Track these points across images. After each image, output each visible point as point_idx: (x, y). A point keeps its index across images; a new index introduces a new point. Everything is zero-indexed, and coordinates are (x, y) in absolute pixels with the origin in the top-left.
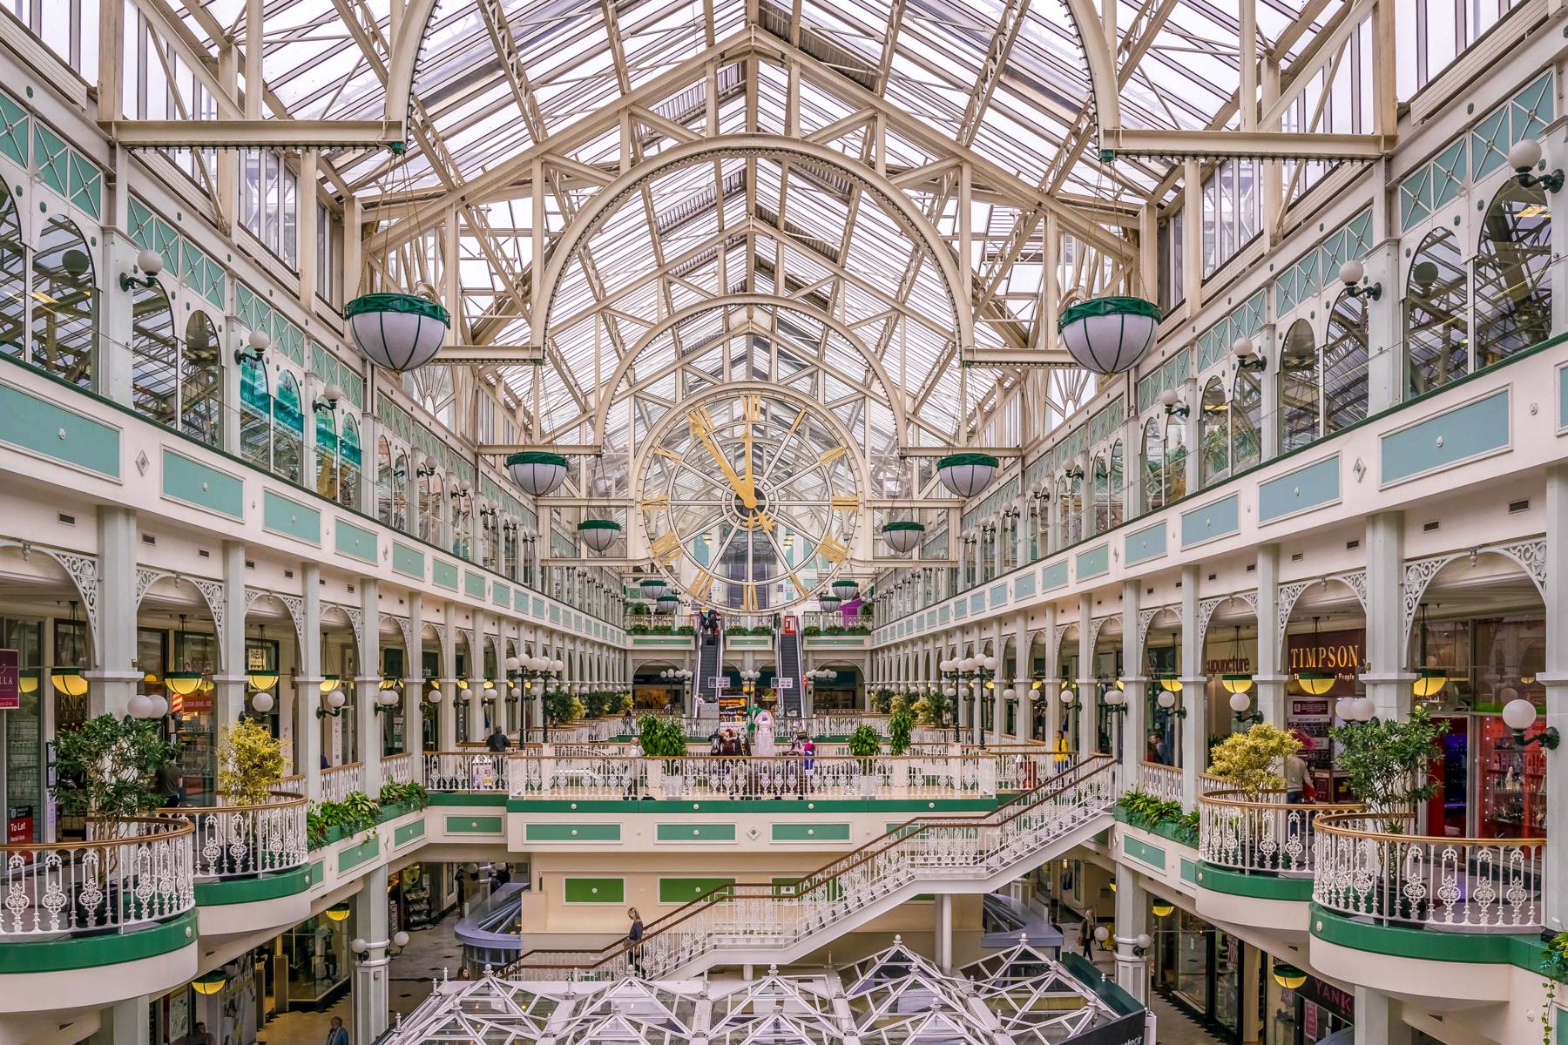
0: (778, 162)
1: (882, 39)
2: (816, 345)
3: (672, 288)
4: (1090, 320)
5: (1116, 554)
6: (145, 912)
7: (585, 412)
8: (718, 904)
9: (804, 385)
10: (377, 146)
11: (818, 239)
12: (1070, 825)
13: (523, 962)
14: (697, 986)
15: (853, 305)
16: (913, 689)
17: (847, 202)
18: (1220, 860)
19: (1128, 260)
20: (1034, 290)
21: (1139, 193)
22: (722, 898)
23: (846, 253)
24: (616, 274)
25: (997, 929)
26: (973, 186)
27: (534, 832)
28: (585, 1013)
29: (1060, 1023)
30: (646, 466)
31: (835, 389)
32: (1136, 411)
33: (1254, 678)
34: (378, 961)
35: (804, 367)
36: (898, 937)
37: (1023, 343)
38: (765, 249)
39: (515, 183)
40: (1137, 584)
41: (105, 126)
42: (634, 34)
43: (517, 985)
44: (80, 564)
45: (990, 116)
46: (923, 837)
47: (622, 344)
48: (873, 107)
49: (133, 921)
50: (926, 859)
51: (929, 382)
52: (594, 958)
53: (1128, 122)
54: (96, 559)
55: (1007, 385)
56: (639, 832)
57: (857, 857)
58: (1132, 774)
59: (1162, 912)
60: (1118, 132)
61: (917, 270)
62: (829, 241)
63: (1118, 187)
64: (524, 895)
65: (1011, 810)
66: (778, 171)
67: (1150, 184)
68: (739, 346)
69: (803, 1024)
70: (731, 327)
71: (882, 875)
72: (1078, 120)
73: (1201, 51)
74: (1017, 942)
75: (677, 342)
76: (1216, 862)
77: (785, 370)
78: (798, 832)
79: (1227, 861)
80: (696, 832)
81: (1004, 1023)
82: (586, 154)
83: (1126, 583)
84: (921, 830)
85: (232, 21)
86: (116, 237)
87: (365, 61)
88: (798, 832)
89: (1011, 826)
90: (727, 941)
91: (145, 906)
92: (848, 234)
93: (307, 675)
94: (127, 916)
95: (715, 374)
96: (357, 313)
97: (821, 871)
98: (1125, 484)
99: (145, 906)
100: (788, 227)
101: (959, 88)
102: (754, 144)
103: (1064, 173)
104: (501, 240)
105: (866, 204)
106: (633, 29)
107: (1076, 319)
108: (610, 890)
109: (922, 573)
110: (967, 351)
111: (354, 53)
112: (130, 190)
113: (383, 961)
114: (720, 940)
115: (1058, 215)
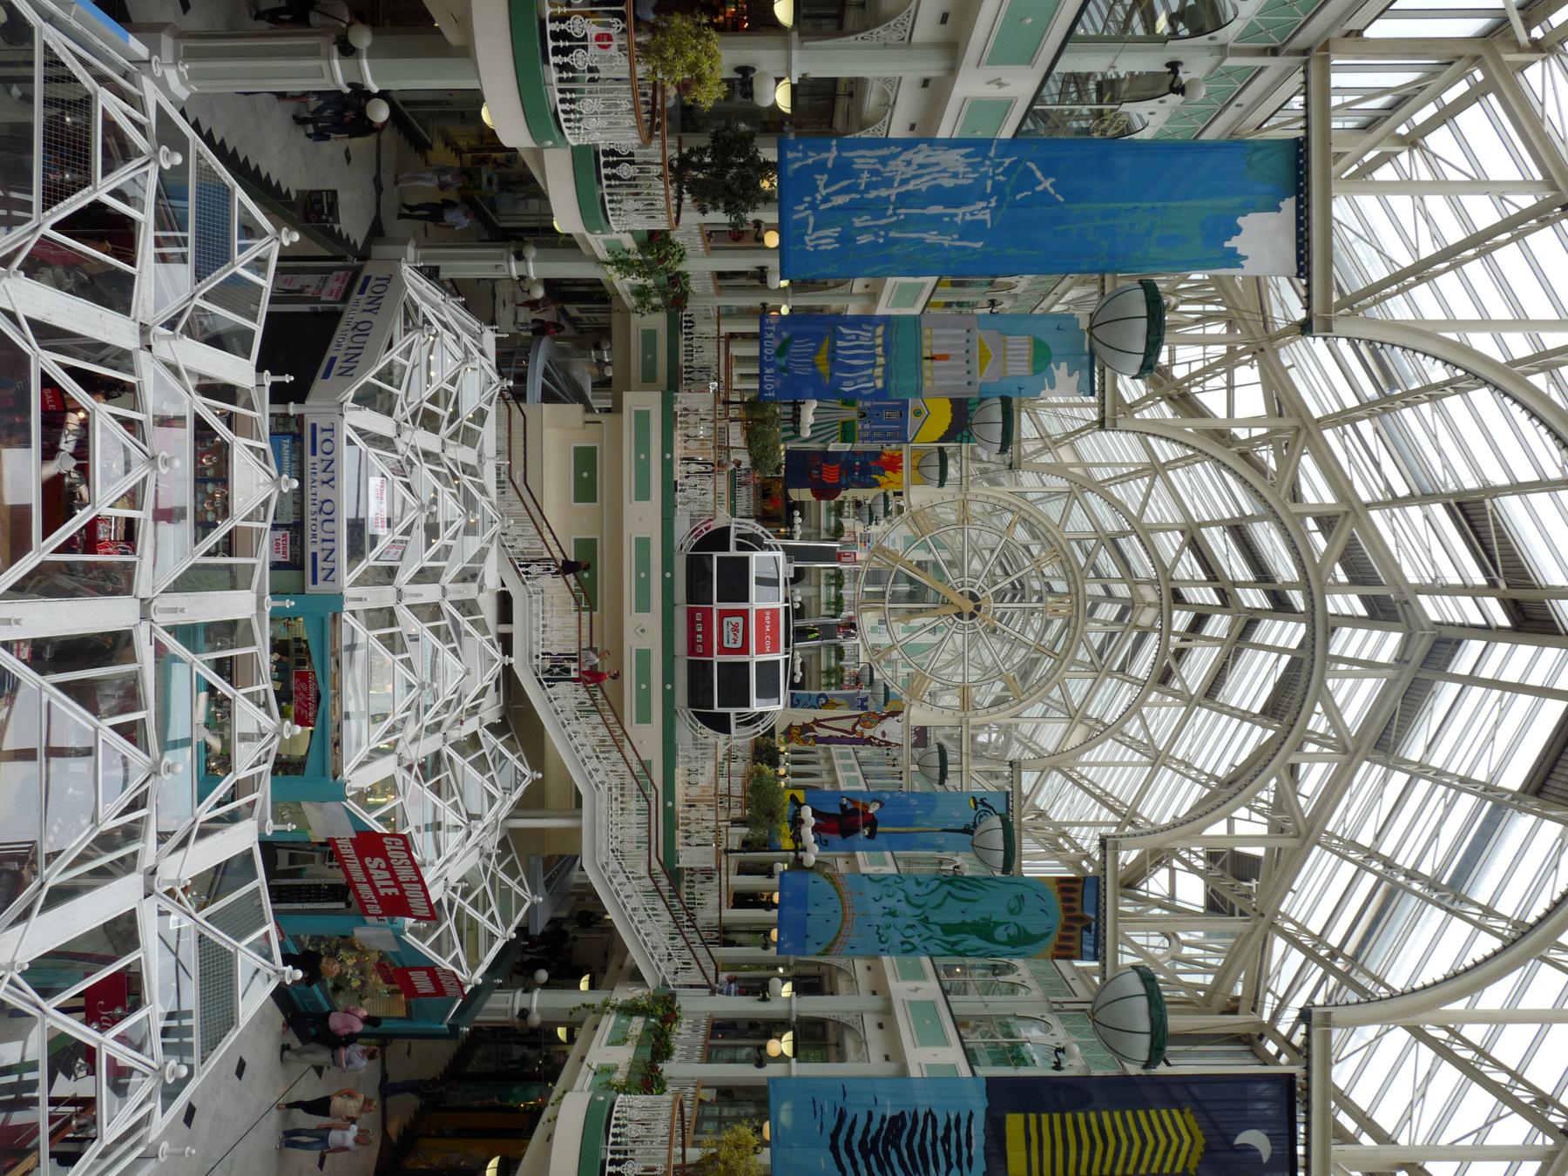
0: (1301, 645)
1: (1423, 762)
2: (1122, 669)
3: (1177, 533)
4: (1144, 1000)
5: (916, 990)
6: (567, 107)
7: (1055, 443)
8: (572, 599)
9: (1083, 655)
10: (1308, 307)
11: (1228, 680)
12: (649, 944)
13: (514, 406)
14: (492, 581)
15: (1162, 717)
16: (782, 759)
17: (1264, 712)
18: (616, 1119)
19: (1207, 1001)
20: (1178, 896)
21: (1276, 1016)
22: (578, 602)
23: (1212, 709)
24: (1190, 481)
25: (546, 869)
26: (1280, 849)
27: (642, 418)
28: (466, 479)
29: (454, 947)
30: (979, 498)
31: (1078, 688)
32: (1058, 1010)
33: (794, 1060)
34: (514, 269)
35: (1100, 656)
36: (540, 775)
37: (1125, 883)
38: (1218, 625)
39: (1281, 397)
40: (888, 1011)
41: (1326, 46)
42: (1426, 517)
43: (492, 410)
44: (901, 28)
45: (1348, 869)
46: (638, 796)
47: (1122, 482)
48: (1357, 750)
49: (558, 96)
50: (616, 799)
51: (1086, 783)
52: (519, 481)
53: (1336, 1034)
54: (907, 42)
55: (1084, 864)
56: (642, 519)
57: (619, 732)
58: (698, 1006)
59: (561, 1033)
60: (1329, 1026)
61: (1196, 781)
62: (1226, 690)
63: (1281, 994)
64: (579, 407)
65: (664, 882)
66: (1294, 645)
67: (1283, 1029)
68: (1121, 590)
69: (455, 696)
70: (1139, 587)
71: (601, 756)
72: (1345, 957)
73: (1415, 1090)
74: (534, 892)
75: (1124, 534)
76: (614, 1115)
77: (1096, 639)
78: (643, 674)
79: (615, 1126)
80: (643, 575)
81: (454, 889)
82: (1307, 462)
83: (889, 999)
84: (644, 795)
85: (1432, 148)
86: (1217, 58)
87: (1398, 269)
88: (643, 674)
89: (648, 882)
90: (536, 608)
91: (573, 107)
92: (1234, 712)
93: (801, 48)
94: (561, 91)
95: (1094, 568)
96: (1146, 293)
97: (605, 696)
98: (986, 998)
99: (573, 107)
100: (1238, 652)
101: (1377, 837)
102: (1322, 626)
103: (1293, 941)
104: (1224, 376)
105: (1258, 735)
106: (1431, 517)
107: (1145, 986)
108: (585, 490)
109: (897, 769)
110: (1116, 843)
111: (1406, 261)
112: (1262, 69)
113: (515, 274)
114: (537, 602)
115: (1251, 933)
